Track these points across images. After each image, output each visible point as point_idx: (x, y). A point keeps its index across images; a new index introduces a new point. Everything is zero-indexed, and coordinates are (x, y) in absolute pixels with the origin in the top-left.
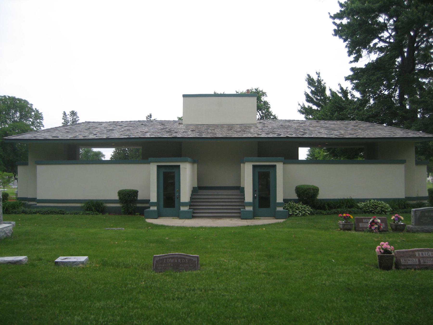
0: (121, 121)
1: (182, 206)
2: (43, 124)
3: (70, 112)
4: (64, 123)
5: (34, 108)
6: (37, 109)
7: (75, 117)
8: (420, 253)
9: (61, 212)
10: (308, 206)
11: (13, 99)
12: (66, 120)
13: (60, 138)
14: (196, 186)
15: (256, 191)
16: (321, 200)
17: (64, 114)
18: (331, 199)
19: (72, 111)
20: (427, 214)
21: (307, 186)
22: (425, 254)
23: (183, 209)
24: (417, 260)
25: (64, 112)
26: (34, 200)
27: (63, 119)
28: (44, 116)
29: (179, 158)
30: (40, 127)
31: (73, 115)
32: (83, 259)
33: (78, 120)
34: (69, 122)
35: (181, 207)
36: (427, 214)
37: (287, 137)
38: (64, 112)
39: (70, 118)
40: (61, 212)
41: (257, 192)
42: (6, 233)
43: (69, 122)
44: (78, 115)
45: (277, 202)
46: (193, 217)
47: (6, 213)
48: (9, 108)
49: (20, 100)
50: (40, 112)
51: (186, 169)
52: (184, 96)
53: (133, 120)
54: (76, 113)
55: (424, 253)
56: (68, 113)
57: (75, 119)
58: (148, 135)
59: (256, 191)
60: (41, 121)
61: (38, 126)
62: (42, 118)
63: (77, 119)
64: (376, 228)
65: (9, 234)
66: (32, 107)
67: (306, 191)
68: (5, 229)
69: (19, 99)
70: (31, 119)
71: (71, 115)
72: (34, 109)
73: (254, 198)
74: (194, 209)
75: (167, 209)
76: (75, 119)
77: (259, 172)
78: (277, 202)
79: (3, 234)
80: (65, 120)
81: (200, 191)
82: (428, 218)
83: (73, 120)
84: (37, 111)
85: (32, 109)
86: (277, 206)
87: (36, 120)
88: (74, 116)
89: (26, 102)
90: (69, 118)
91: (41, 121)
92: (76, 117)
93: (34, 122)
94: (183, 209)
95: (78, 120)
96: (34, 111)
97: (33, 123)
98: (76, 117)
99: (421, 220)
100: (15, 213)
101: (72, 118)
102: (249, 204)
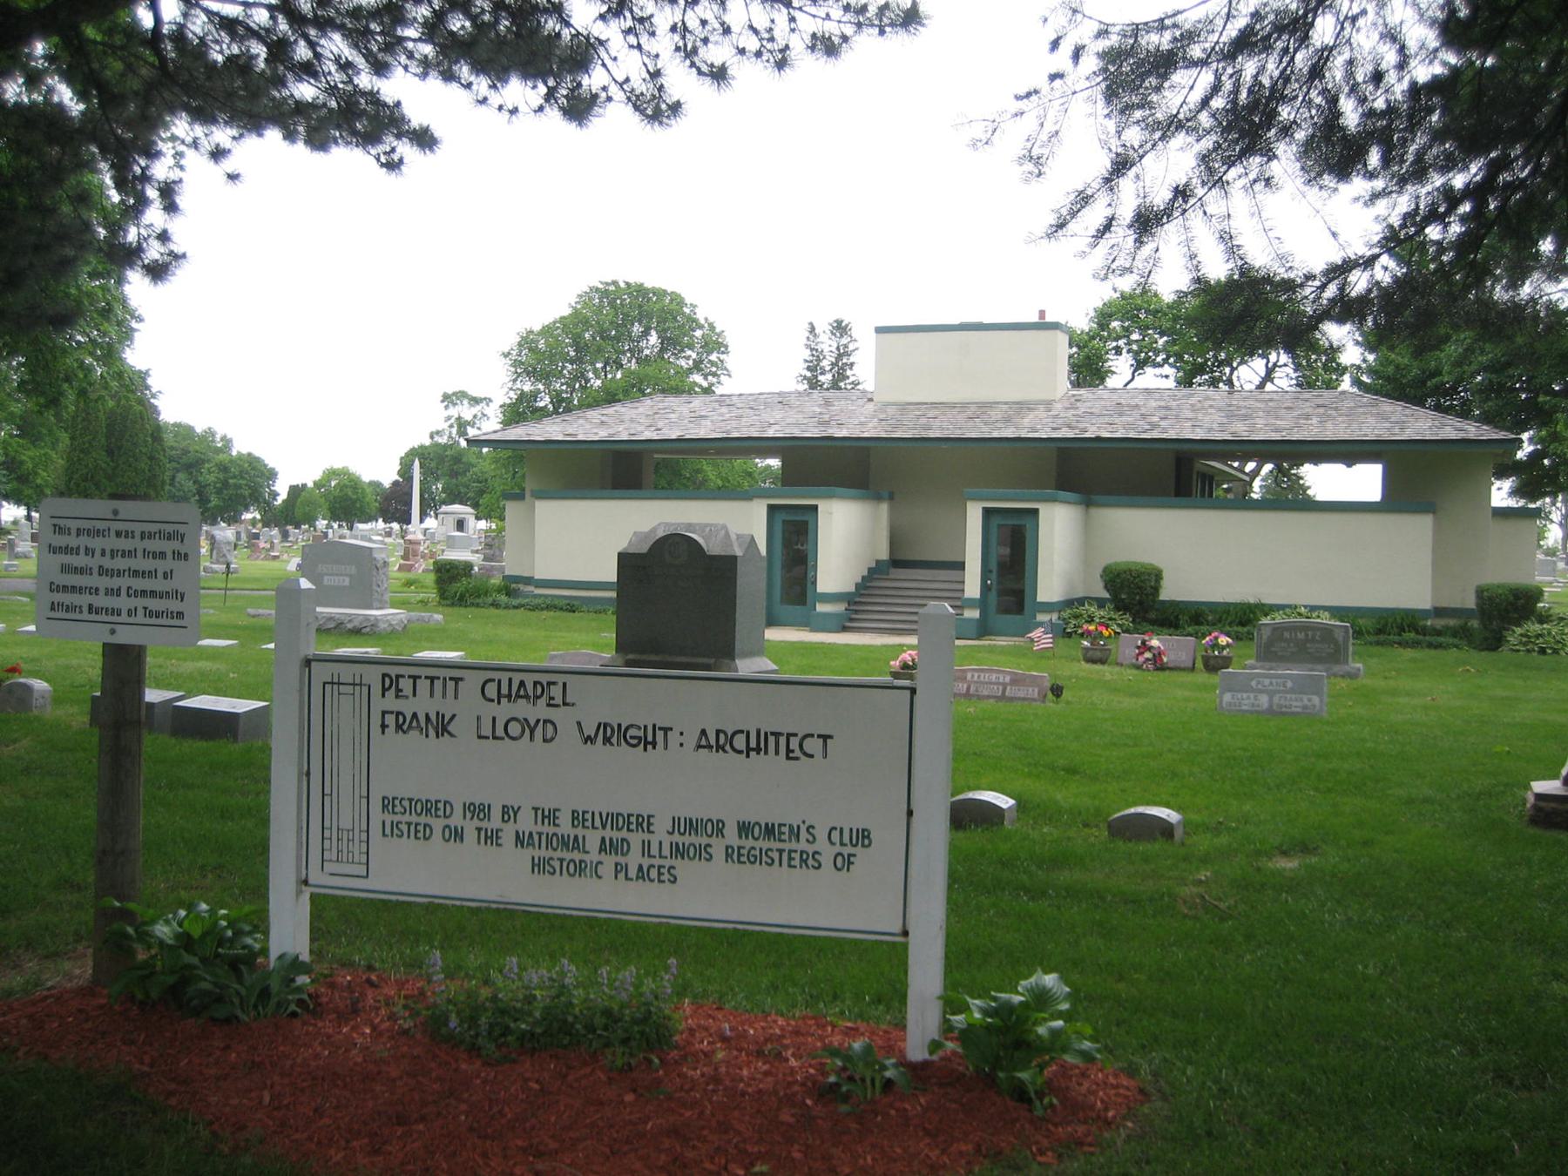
0: (738, 393)
1: (819, 602)
2: (728, 366)
3: (831, 325)
4: (812, 361)
5: (700, 316)
6: (711, 320)
7: (844, 341)
8: (976, 675)
9: (571, 607)
10: (1128, 616)
11: (639, 291)
12: (817, 350)
13: (580, 437)
14: (884, 555)
15: (991, 571)
16: (1164, 602)
17: (811, 332)
18: (1204, 603)
19: (835, 321)
20: (1287, 635)
21: (1143, 565)
22: (985, 677)
23: (821, 608)
24: (965, 686)
25: (811, 324)
26: (529, 581)
27: (808, 346)
28: (730, 339)
29: (638, 491)
30: (719, 376)
31: (838, 334)
32: (319, 609)
33: (854, 351)
34: (824, 358)
35: (817, 605)
36: (1287, 635)
37: (1098, 439)
38: (811, 324)
39: (830, 342)
40: (571, 607)
41: (994, 575)
42: (391, 625)
43: (824, 358)
44: (854, 333)
45: (1038, 600)
46: (845, 629)
47: (461, 605)
48: (628, 321)
49: (660, 293)
50: (718, 330)
51: (831, 513)
52: (879, 330)
53: (767, 391)
54: (847, 325)
55: (982, 675)
56: (823, 327)
57: (846, 346)
58: (771, 433)
59: (991, 571)
60: (722, 357)
61: (714, 375)
62: (726, 347)
63: (851, 347)
64: (1147, 659)
65: (397, 627)
66: (695, 314)
67: (1118, 575)
68: (389, 618)
69: (656, 292)
70: (689, 353)
71: (832, 332)
72: (702, 322)
73: (985, 588)
74: (856, 612)
75: (790, 608)
76: (846, 346)
77: (784, 521)
78: (1038, 600)
79: (386, 626)
80: (812, 350)
81: (892, 570)
82: (1292, 645)
83: (838, 349)
84: (712, 327)
85: (695, 321)
86: (1039, 612)
87: (709, 353)
88: (842, 336)
89: (677, 300)
90: (828, 344)
91: (722, 357)
92: (849, 339)
93: (701, 361)
94: (821, 608)
95: (854, 351)
96: (701, 327)
97: (697, 366)
98: (849, 339)
99: (1273, 649)
100: (478, 605)
101: (836, 345)
102: (971, 603)
